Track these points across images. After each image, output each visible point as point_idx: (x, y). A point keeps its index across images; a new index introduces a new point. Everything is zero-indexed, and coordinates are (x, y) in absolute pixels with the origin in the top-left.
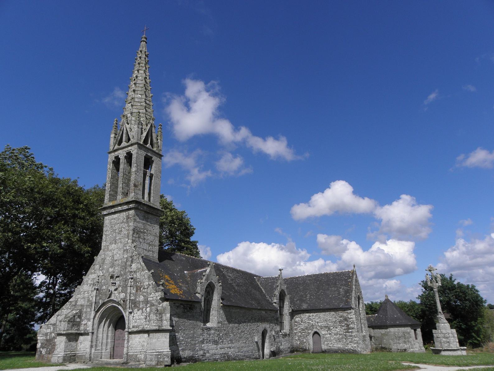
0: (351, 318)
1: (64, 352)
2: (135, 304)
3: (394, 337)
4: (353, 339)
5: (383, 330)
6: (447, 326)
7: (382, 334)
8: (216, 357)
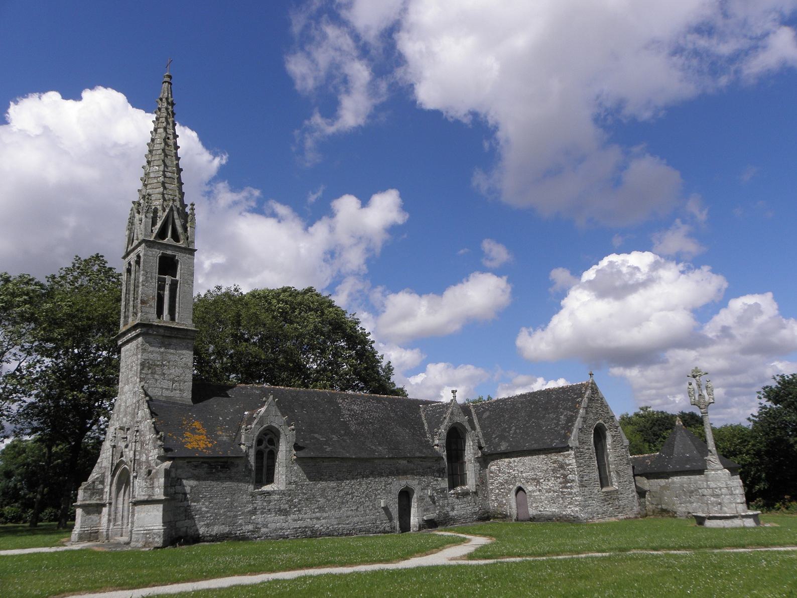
0: (570, 465)
1: (81, 528)
3: (681, 491)
4: (574, 499)
5: (663, 480)
7: (661, 487)
8: (284, 533)
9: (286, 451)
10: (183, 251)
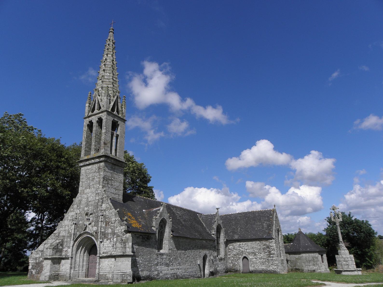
0: (272, 246)
1: (50, 272)
2: (105, 235)
3: (306, 261)
4: (274, 262)
5: (297, 255)
6: (347, 252)
7: (296, 258)
8: (167, 276)
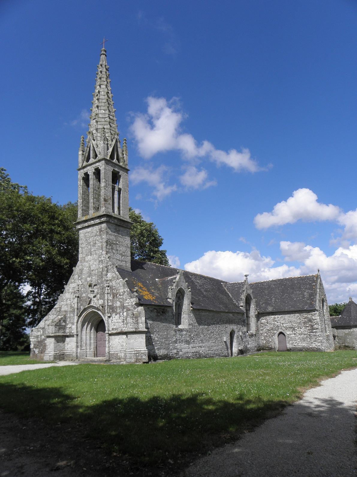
0: (315, 319)
4: (317, 338)
9: (188, 304)
10: (123, 170)
